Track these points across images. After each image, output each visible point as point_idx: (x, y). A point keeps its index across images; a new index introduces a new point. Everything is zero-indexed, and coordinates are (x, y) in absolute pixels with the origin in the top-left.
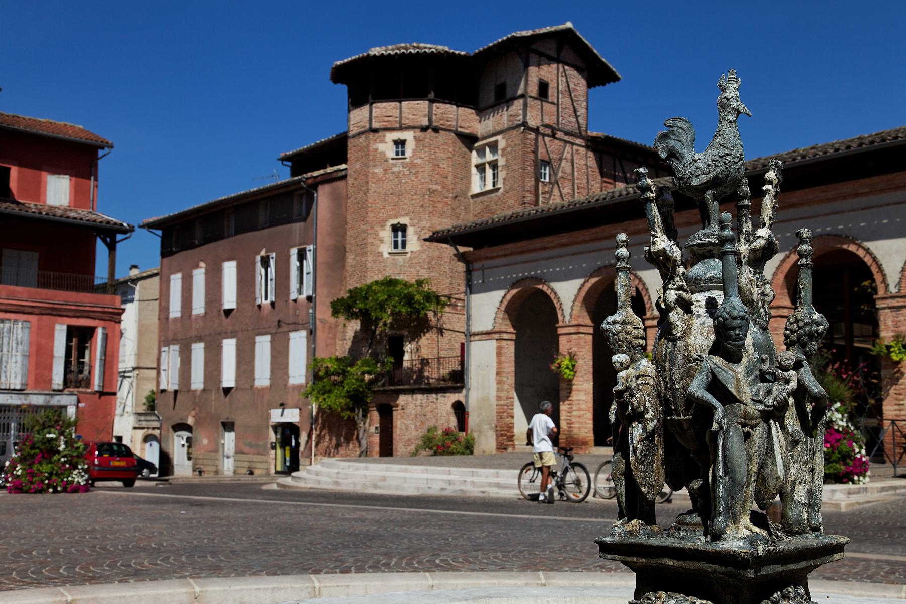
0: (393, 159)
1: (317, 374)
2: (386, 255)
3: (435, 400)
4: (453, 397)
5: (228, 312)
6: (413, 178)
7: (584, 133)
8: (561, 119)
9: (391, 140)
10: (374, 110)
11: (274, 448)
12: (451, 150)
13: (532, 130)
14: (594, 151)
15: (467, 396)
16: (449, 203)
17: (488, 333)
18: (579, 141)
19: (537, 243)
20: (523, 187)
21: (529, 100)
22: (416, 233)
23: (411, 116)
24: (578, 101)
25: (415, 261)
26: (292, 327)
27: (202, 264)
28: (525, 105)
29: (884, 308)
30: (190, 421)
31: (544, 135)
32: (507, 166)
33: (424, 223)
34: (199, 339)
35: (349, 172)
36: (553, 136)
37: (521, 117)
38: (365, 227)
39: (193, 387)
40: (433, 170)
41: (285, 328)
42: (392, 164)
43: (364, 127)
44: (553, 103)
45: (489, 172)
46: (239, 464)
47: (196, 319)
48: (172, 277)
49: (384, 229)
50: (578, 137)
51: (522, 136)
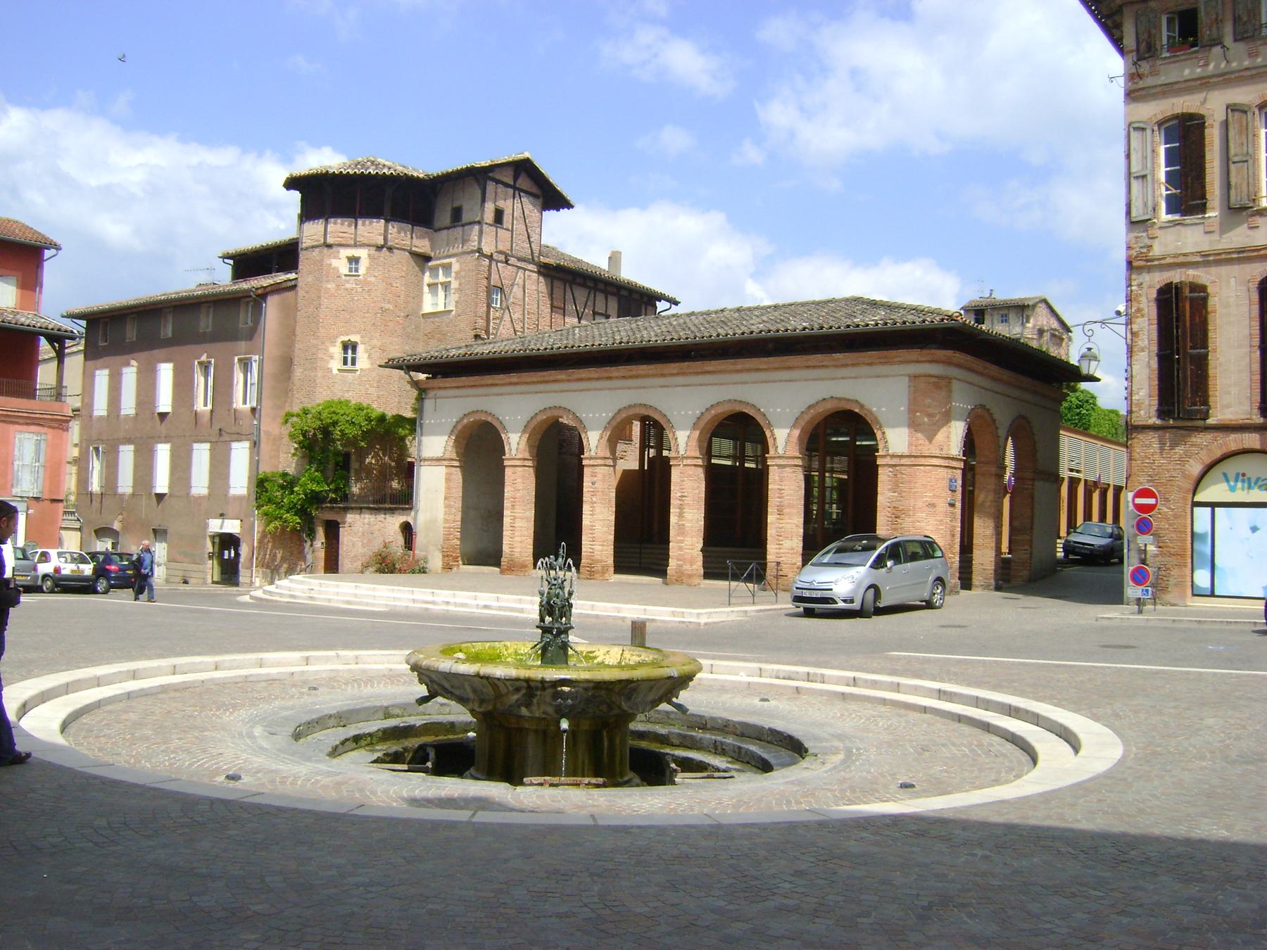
0: (345, 275)
1: (261, 484)
2: (335, 372)
3: (383, 520)
4: (400, 519)
5: (163, 416)
7: (536, 259)
8: (514, 245)
11: (211, 557)
13: (486, 256)
14: (544, 275)
15: (415, 519)
17: (438, 460)
18: (532, 267)
19: (489, 379)
20: (475, 313)
21: (485, 227)
23: (366, 234)
25: (364, 379)
26: (234, 437)
27: (134, 363)
28: (481, 232)
29: (774, 465)
30: (117, 526)
31: (497, 262)
32: (460, 290)
33: (375, 342)
34: (128, 441)
35: (300, 284)
36: (506, 262)
37: (476, 243)
38: (315, 342)
39: (120, 490)
40: (386, 289)
41: (226, 438)
42: (345, 280)
43: (317, 241)
44: (508, 230)
45: (441, 293)
46: (173, 572)
47: (125, 419)
48: (98, 372)
49: (335, 346)
50: (530, 263)
51: (476, 263)
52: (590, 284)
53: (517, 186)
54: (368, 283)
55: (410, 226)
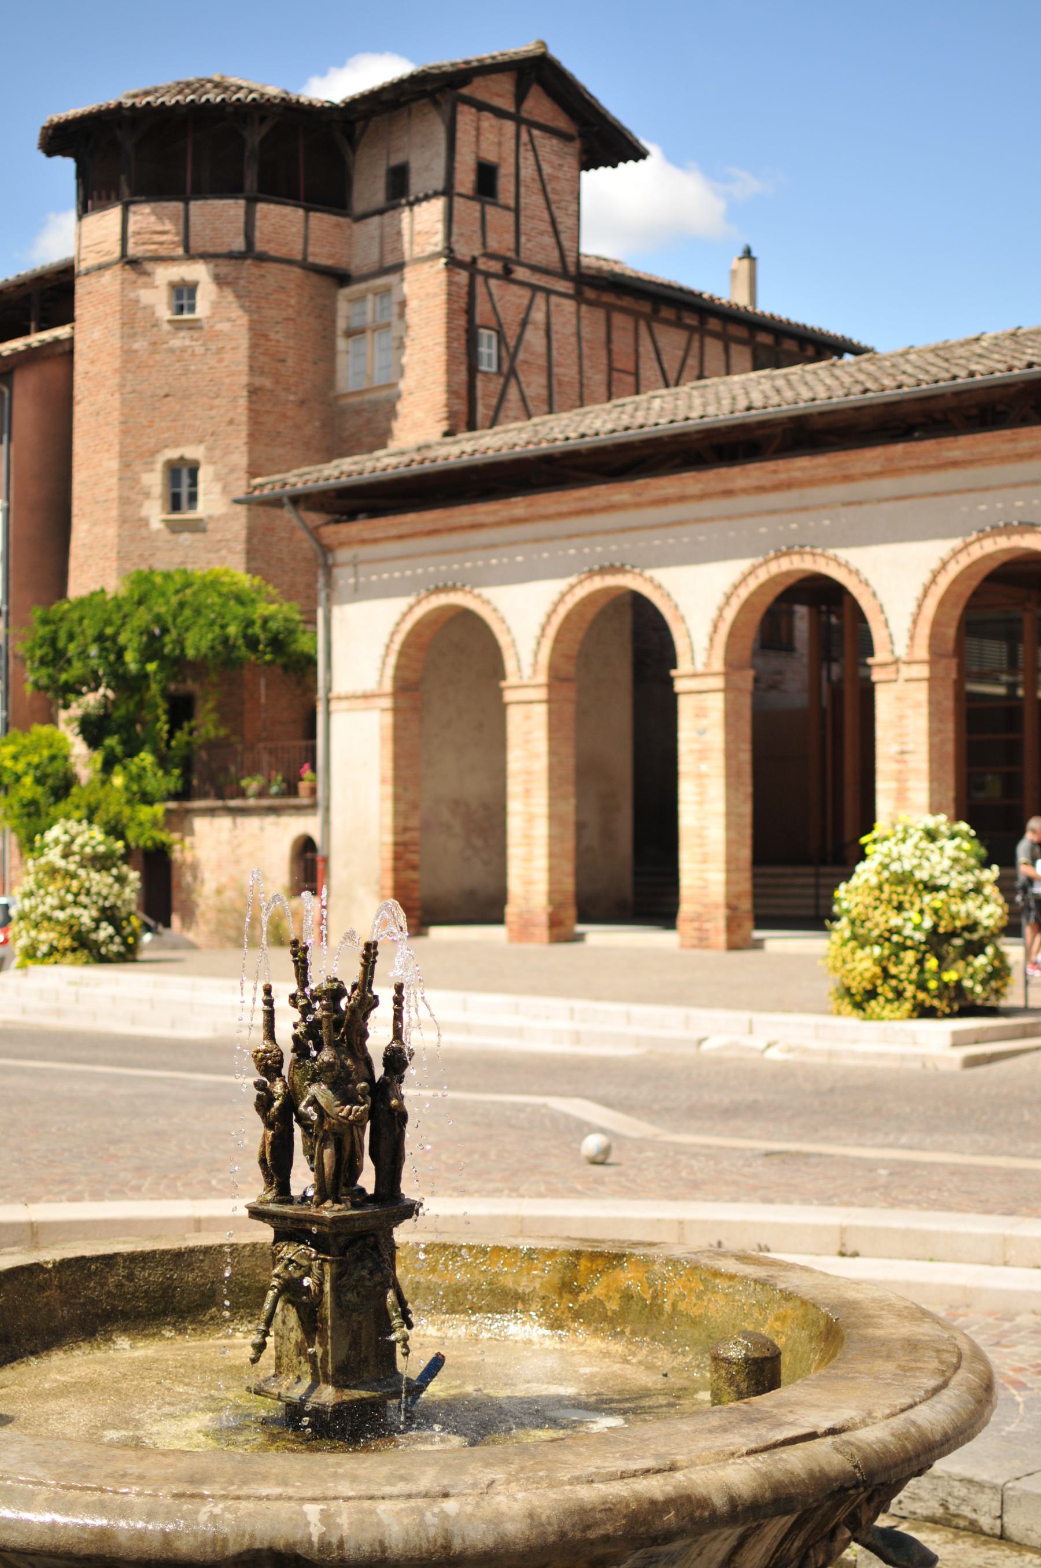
6: (213, 362)
8: (523, 239)
9: (165, 282)
10: (132, 219)
12: (293, 301)
16: (290, 413)
17: (366, 696)
22: (217, 478)
24: (560, 201)
43: (107, 253)
44: (506, 208)
52: (691, 320)
53: (524, 114)
54: (217, 335)
55: (301, 212)
